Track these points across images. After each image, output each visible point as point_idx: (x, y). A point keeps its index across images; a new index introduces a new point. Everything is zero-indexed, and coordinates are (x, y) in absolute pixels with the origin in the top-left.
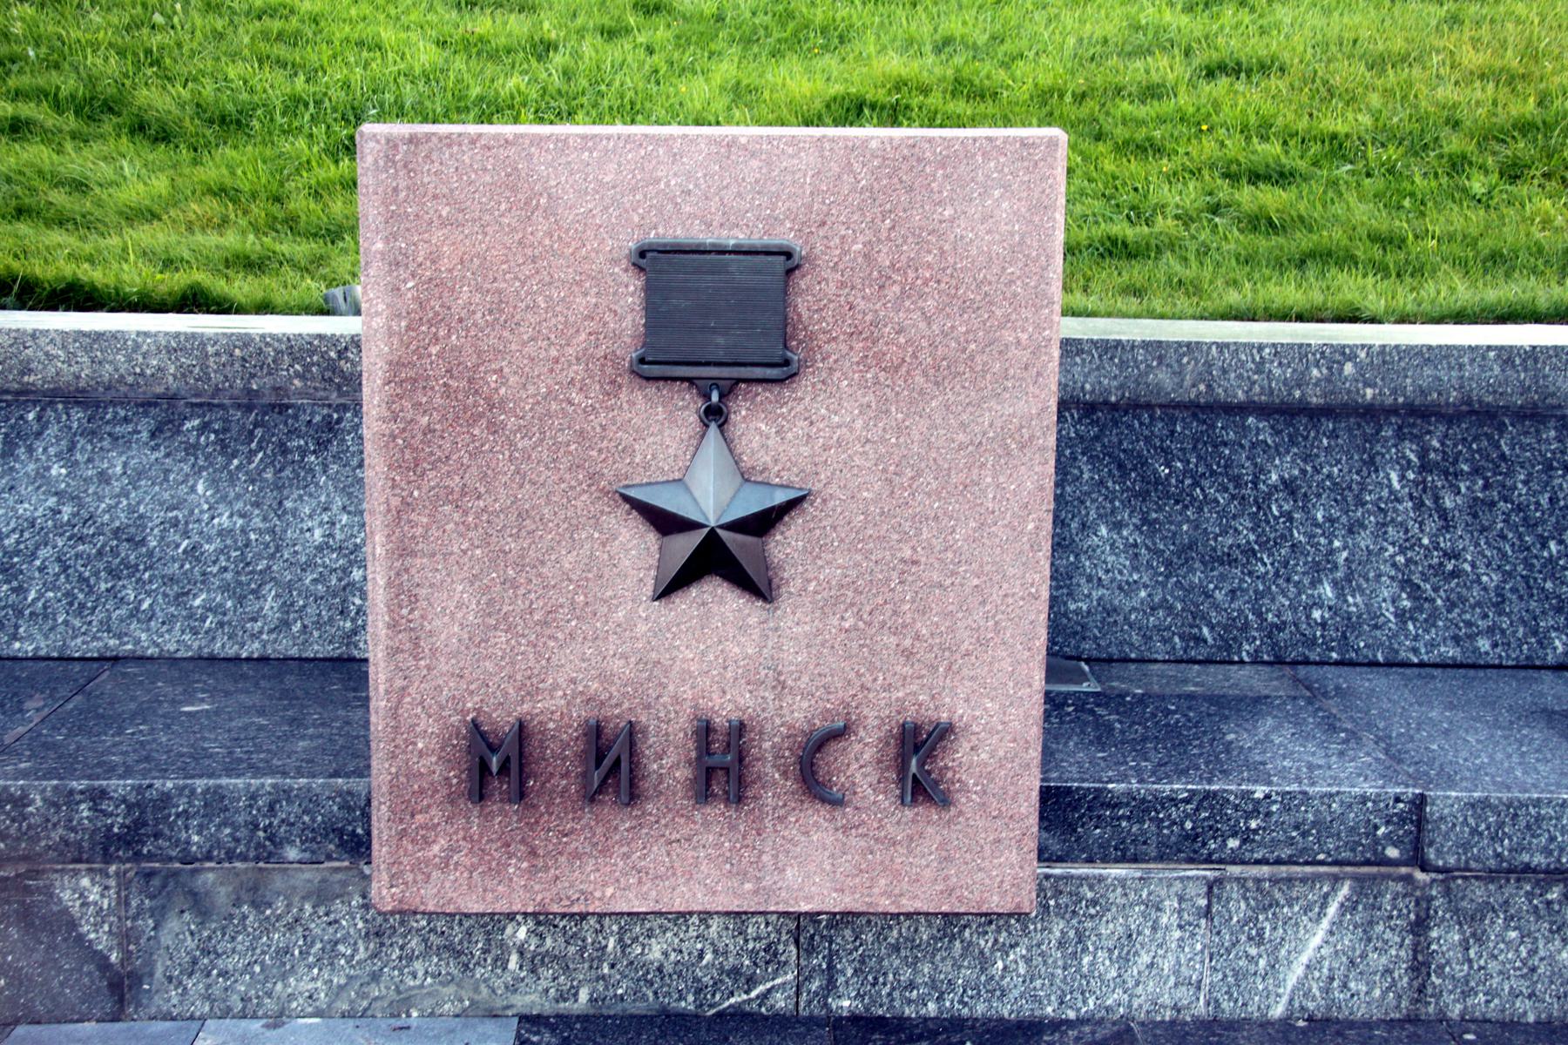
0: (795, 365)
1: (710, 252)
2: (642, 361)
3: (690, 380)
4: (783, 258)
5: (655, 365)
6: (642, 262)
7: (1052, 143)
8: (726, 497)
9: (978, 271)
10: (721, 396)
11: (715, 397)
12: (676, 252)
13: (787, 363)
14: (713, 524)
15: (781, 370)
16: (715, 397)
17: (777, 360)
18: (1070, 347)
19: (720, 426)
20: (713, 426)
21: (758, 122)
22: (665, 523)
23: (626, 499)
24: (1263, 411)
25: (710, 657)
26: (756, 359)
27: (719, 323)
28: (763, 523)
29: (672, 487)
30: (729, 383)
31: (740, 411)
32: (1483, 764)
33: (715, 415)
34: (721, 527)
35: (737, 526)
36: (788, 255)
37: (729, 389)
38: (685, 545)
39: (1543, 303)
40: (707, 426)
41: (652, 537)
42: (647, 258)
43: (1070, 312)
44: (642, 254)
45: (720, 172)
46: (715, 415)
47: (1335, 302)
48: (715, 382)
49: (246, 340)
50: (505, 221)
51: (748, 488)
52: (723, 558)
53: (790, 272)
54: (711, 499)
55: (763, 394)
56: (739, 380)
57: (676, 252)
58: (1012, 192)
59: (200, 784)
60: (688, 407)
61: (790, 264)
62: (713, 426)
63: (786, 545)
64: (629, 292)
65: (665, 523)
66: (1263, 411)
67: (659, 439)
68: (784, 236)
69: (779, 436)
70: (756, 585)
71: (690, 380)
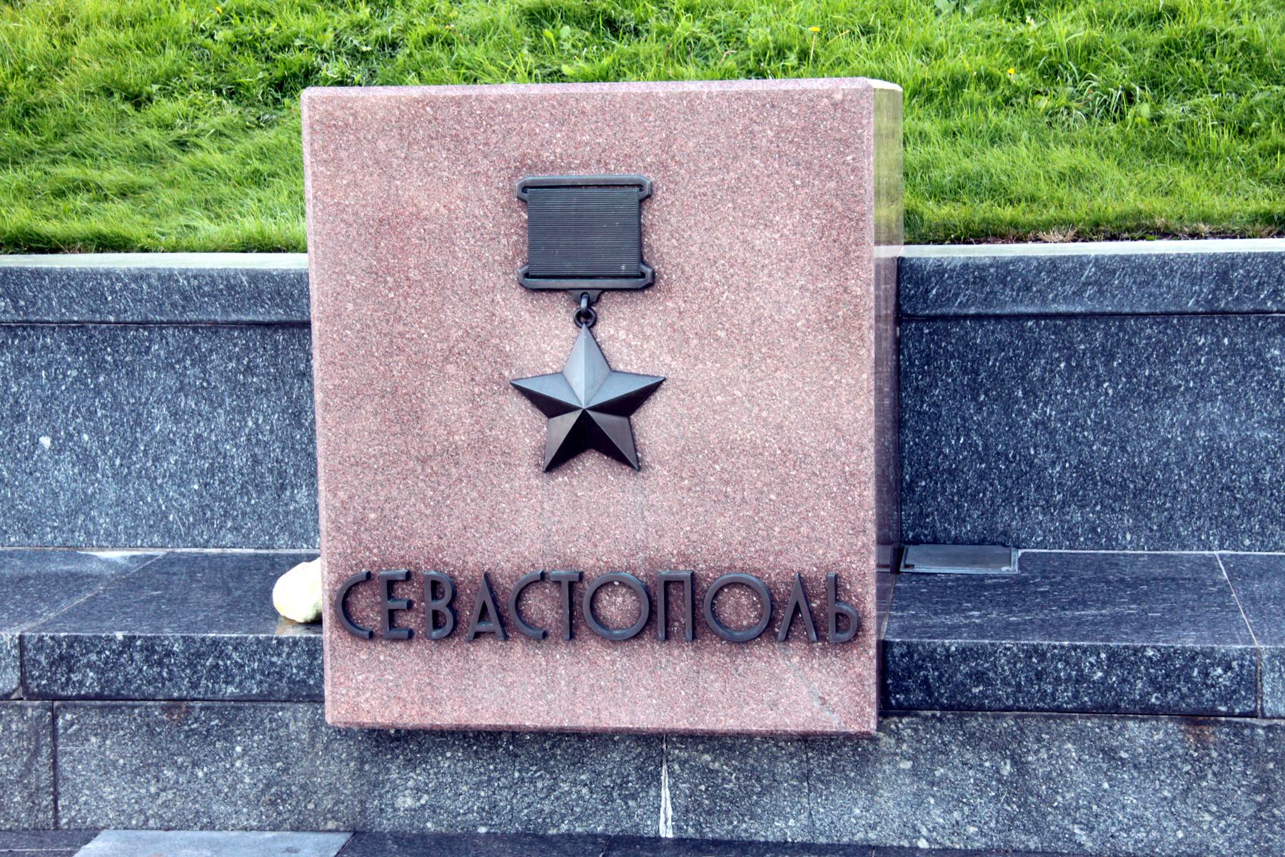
1: (580, 186)
2: (527, 275)
4: (636, 189)
5: (537, 279)
6: (525, 196)
10: (590, 304)
11: (584, 304)
12: (586, 186)
13: (643, 275)
15: (642, 281)
17: (634, 273)
19: (589, 328)
22: (550, 407)
23: (517, 387)
26: (570, 273)
28: (628, 405)
30: (598, 292)
31: (601, 310)
33: (586, 318)
35: (603, 408)
36: (640, 186)
38: (566, 423)
44: (525, 188)
45: (592, 119)
46: (586, 318)
48: (584, 292)
49: (167, 278)
50: (373, 203)
51: (615, 377)
52: (595, 435)
53: (642, 201)
54: (582, 389)
56: (604, 290)
57: (586, 186)
63: (652, 425)
65: (550, 407)
67: (550, 347)
69: (635, 337)
70: (623, 456)
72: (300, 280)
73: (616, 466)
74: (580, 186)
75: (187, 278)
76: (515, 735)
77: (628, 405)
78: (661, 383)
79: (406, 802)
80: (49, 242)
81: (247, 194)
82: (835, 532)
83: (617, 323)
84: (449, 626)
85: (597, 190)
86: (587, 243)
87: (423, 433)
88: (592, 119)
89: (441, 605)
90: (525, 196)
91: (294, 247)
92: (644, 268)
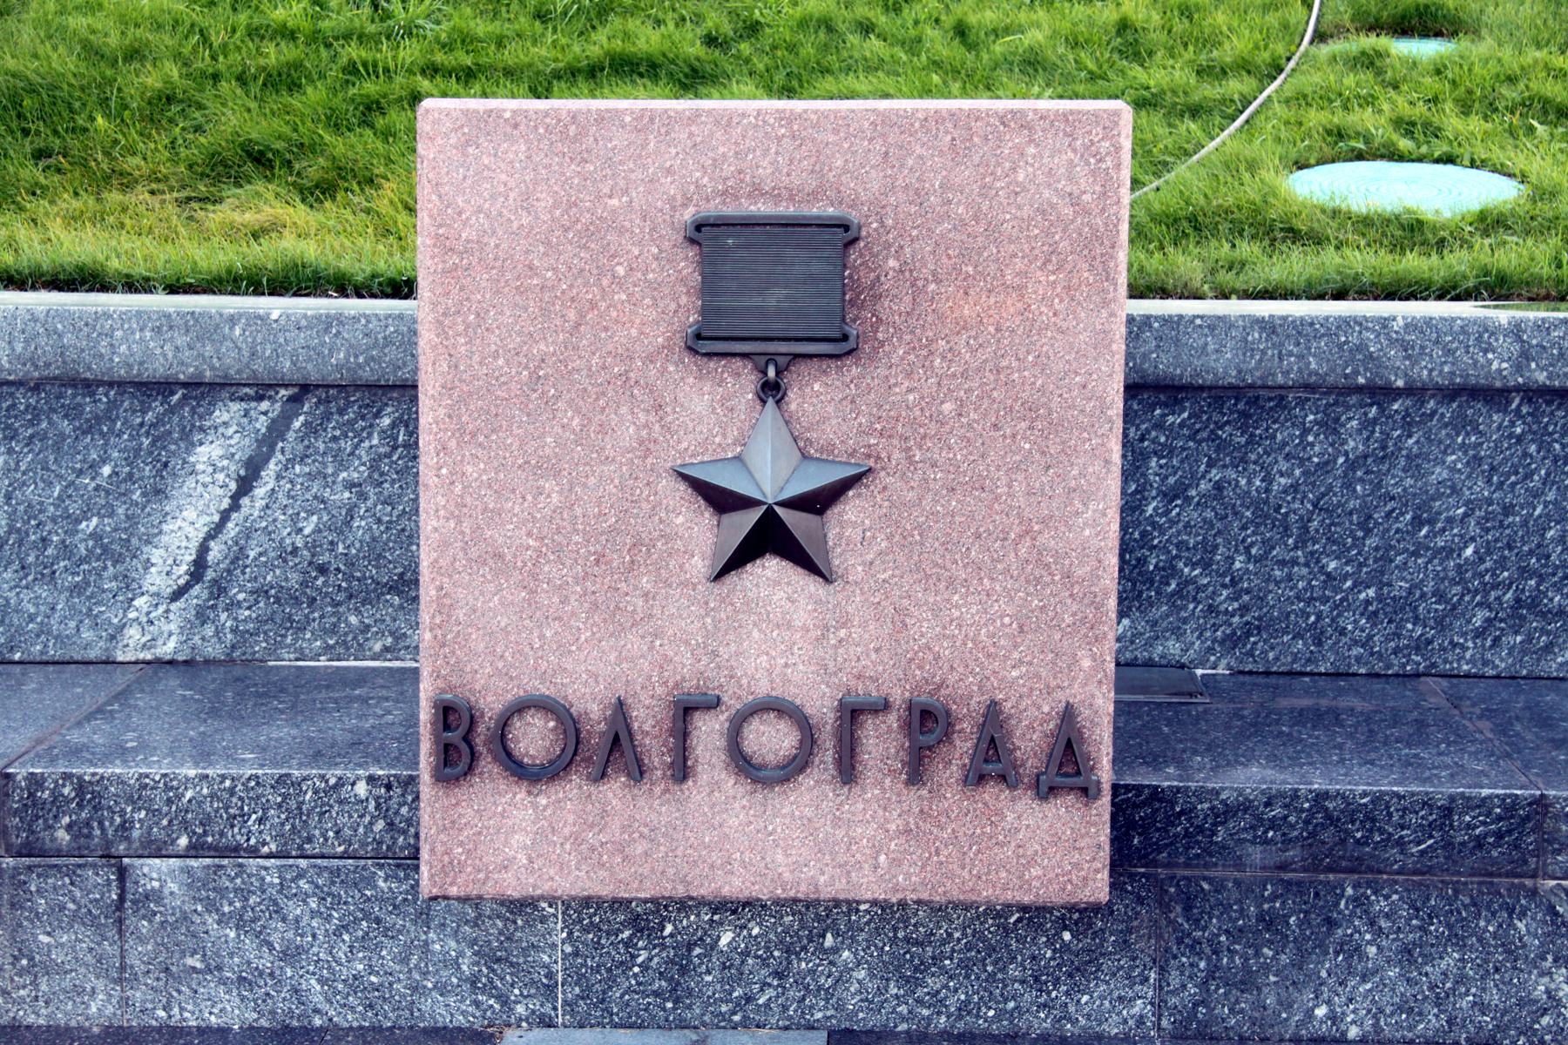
0: (852, 340)
5: (707, 342)
7: (1117, 113)
8: (785, 474)
9: (1024, 215)
10: (778, 373)
11: (771, 373)
13: (845, 338)
14: (770, 501)
15: (840, 346)
16: (771, 373)
17: (837, 335)
18: (1137, 326)
19: (778, 402)
20: (771, 401)
22: (721, 501)
26: (801, 334)
28: (819, 502)
32: (1559, 61)
33: (771, 391)
34: (783, 504)
36: (846, 228)
38: (747, 520)
39: (359, 270)
40: (764, 402)
41: (708, 516)
42: (702, 232)
43: (1136, 292)
44: (699, 227)
45: (746, 144)
46: (771, 391)
47: (268, 254)
48: (771, 358)
52: (776, 539)
54: (771, 476)
57: (787, 225)
58: (1072, 155)
60: (741, 383)
62: (771, 401)
64: (686, 265)
65: (721, 501)
67: (713, 415)
75: (76, 330)
77: (819, 502)
78: (685, 478)
81: (1531, 129)
82: (1059, 657)
83: (817, 395)
84: (466, 759)
86: (779, 293)
87: (548, 538)
88: (746, 144)
89: (454, 736)
90: (696, 236)
91: (402, 288)
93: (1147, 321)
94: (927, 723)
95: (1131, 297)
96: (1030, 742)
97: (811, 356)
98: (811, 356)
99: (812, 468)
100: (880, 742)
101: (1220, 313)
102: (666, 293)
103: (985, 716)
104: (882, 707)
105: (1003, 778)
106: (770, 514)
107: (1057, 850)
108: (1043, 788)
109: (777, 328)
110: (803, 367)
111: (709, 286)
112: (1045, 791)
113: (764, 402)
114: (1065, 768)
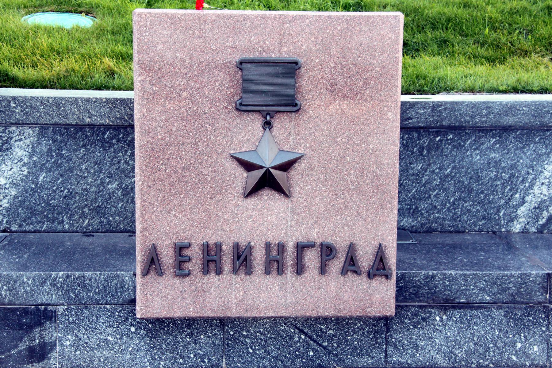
3: (259, 111)
5: (244, 106)
13: (296, 105)
15: (293, 107)
16: (268, 118)
17: (293, 104)
21: (217, 9)
22: (249, 167)
23: (233, 157)
24: (482, 306)
25: (267, 221)
26: (251, 103)
27: (268, 89)
28: (286, 167)
29: (253, 152)
31: (276, 123)
33: (268, 125)
35: (276, 168)
36: (296, 63)
37: (272, 114)
38: (258, 174)
43: (405, 92)
44: (241, 63)
45: (267, 33)
46: (268, 125)
52: (268, 182)
54: (268, 158)
55: (285, 116)
59: (77, 274)
61: (297, 67)
62: (268, 129)
63: (296, 179)
65: (249, 167)
66: (482, 306)
68: (295, 58)
71: (259, 111)
72: (128, 103)
73: (282, 196)
74: (261, 62)
76: (174, 321)
79: (536, 348)
80: (25, 82)
82: (378, 229)
85: (273, 64)
90: (240, 67)
92: (297, 102)
93: (412, 105)
94: (328, 251)
95: (402, 94)
96: (366, 259)
97: (283, 112)
98: (283, 112)
99: (283, 154)
100: (312, 258)
101: (98, 97)
102: (223, 86)
103: (349, 248)
104: (311, 246)
105: (355, 272)
106: (268, 172)
107: (381, 297)
108: (371, 275)
109: (260, 101)
110: (278, 116)
111: (245, 87)
112: (370, 276)
113: (264, 129)
114: (379, 268)
